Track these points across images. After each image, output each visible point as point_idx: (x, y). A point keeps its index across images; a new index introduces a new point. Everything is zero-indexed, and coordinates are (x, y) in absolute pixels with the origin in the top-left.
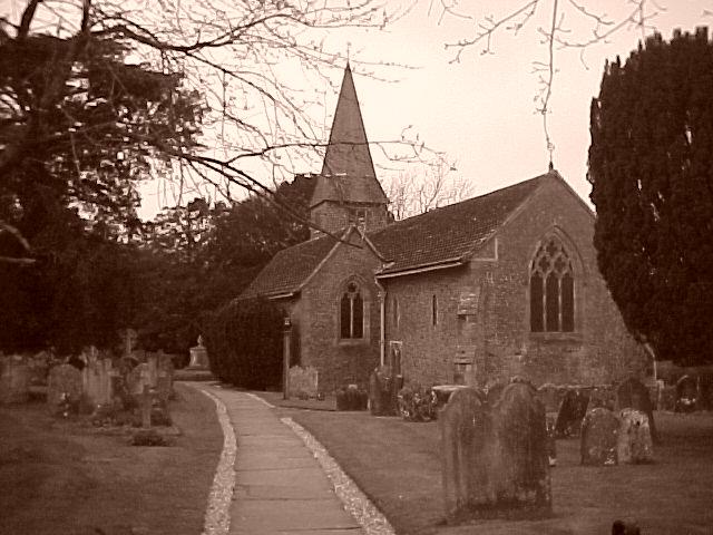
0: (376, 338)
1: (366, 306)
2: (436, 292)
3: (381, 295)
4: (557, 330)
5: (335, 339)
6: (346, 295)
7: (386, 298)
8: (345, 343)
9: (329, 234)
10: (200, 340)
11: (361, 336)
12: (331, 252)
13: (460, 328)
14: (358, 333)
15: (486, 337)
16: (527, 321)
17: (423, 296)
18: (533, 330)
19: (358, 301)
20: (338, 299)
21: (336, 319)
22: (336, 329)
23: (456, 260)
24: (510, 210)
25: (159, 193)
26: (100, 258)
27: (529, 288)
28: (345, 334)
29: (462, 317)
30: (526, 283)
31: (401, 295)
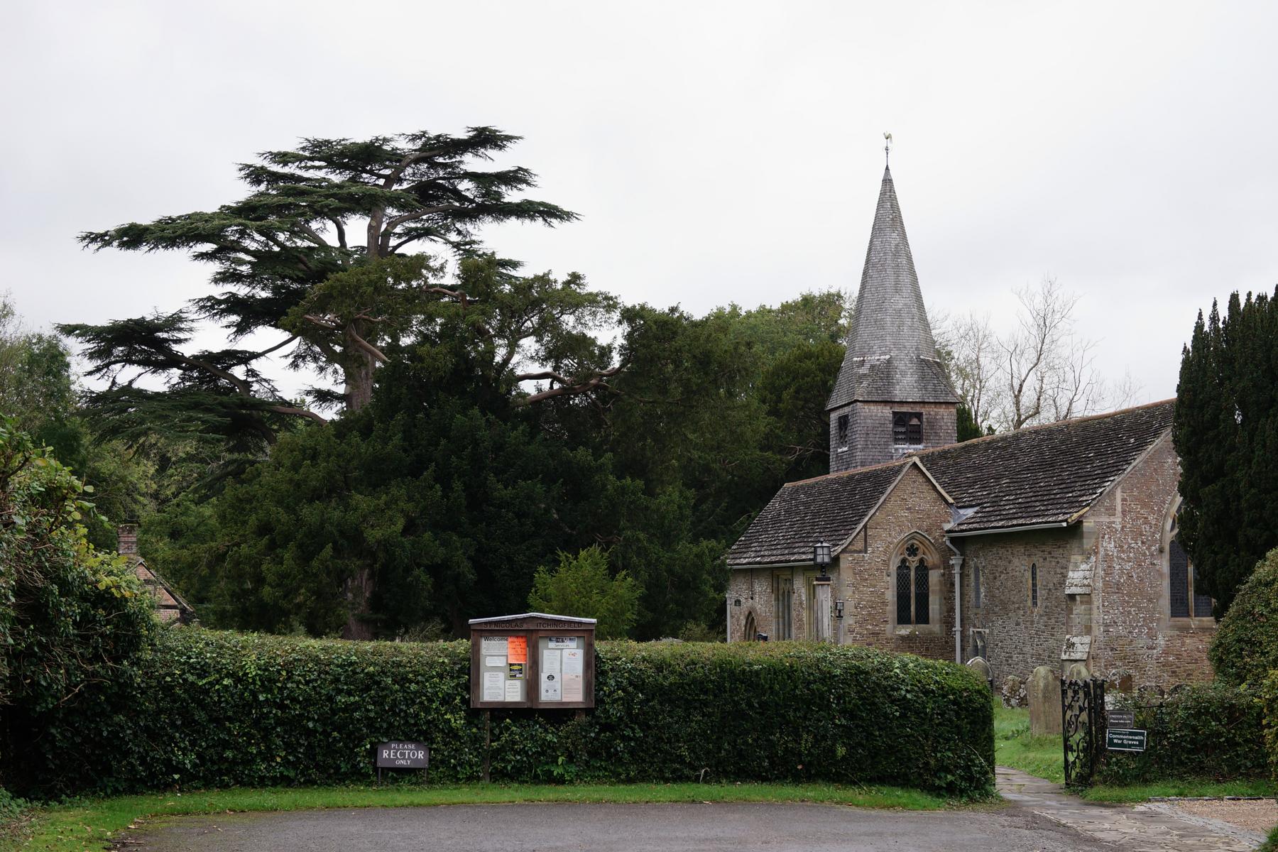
0: (948, 622)
1: (934, 577)
2: (1034, 559)
3: (955, 561)
4: (1188, 615)
5: (889, 627)
6: (904, 561)
7: (962, 567)
8: (905, 631)
9: (14, 473)
10: (412, 249)
11: (927, 622)
12: (889, 490)
13: (1071, 611)
14: (923, 617)
15: (1106, 625)
16: (1165, 602)
17: (1019, 563)
18: (1175, 613)
19: (923, 569)
20: (894, 564)
21: (891, 596)
22: (892, 609)
23: (1063, 519)
24: (1140, 447)
25: (616, 361)
26: (244, 523)
27: (1167, 555)
28: (903, 618)
29: (1072, 597)
30: (1161, 551)
31: (980, 560)
